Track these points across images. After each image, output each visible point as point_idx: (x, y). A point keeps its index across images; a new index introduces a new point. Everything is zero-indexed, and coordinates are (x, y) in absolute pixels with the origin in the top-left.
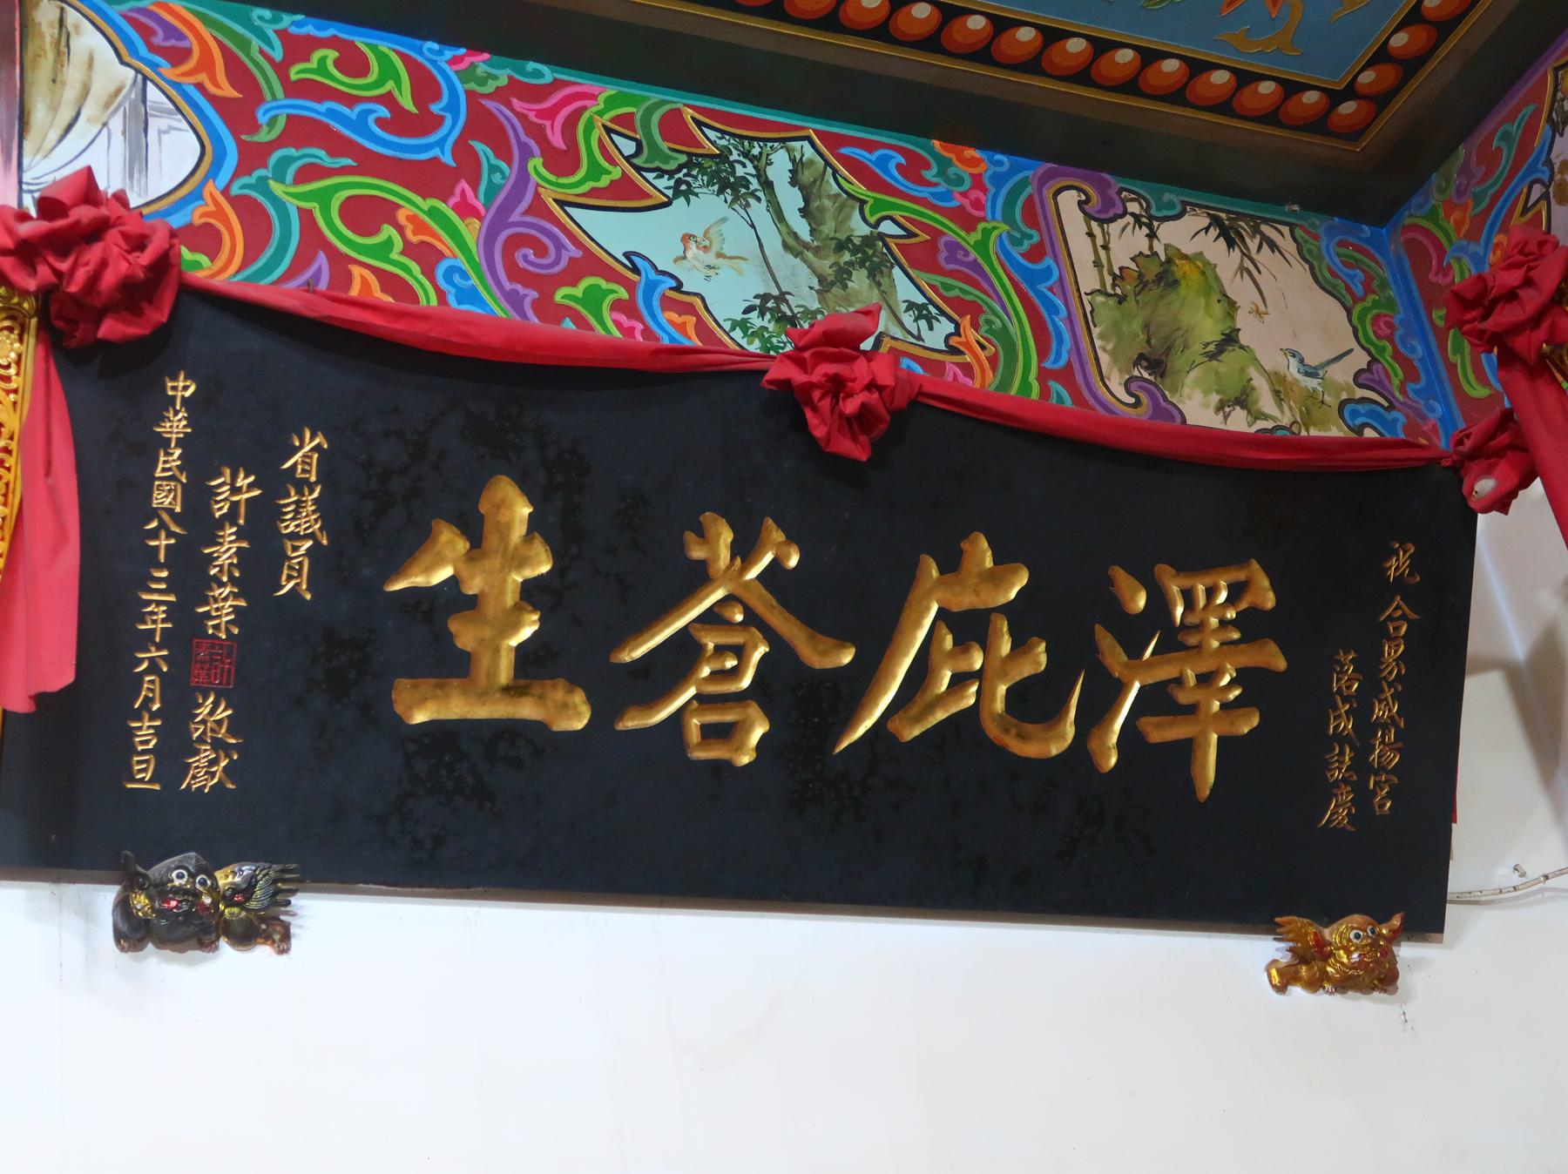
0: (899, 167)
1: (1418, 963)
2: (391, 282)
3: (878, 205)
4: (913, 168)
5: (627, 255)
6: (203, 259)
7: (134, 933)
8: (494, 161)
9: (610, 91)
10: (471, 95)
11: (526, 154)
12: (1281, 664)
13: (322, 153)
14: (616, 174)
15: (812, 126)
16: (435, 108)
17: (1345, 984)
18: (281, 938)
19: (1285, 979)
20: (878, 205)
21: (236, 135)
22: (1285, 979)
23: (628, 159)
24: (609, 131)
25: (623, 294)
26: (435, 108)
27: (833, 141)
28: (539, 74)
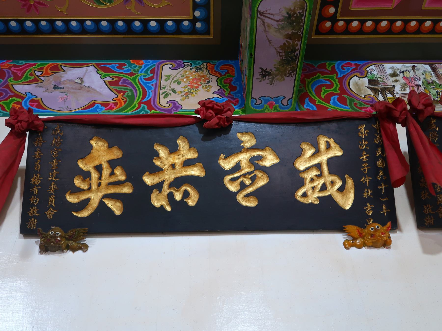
5: (25, 93)
15: (94, 62)
18: (84, 248)
20: (105, 75)
22: (347, 245)
23: (38, 76)
25: (20, 100)
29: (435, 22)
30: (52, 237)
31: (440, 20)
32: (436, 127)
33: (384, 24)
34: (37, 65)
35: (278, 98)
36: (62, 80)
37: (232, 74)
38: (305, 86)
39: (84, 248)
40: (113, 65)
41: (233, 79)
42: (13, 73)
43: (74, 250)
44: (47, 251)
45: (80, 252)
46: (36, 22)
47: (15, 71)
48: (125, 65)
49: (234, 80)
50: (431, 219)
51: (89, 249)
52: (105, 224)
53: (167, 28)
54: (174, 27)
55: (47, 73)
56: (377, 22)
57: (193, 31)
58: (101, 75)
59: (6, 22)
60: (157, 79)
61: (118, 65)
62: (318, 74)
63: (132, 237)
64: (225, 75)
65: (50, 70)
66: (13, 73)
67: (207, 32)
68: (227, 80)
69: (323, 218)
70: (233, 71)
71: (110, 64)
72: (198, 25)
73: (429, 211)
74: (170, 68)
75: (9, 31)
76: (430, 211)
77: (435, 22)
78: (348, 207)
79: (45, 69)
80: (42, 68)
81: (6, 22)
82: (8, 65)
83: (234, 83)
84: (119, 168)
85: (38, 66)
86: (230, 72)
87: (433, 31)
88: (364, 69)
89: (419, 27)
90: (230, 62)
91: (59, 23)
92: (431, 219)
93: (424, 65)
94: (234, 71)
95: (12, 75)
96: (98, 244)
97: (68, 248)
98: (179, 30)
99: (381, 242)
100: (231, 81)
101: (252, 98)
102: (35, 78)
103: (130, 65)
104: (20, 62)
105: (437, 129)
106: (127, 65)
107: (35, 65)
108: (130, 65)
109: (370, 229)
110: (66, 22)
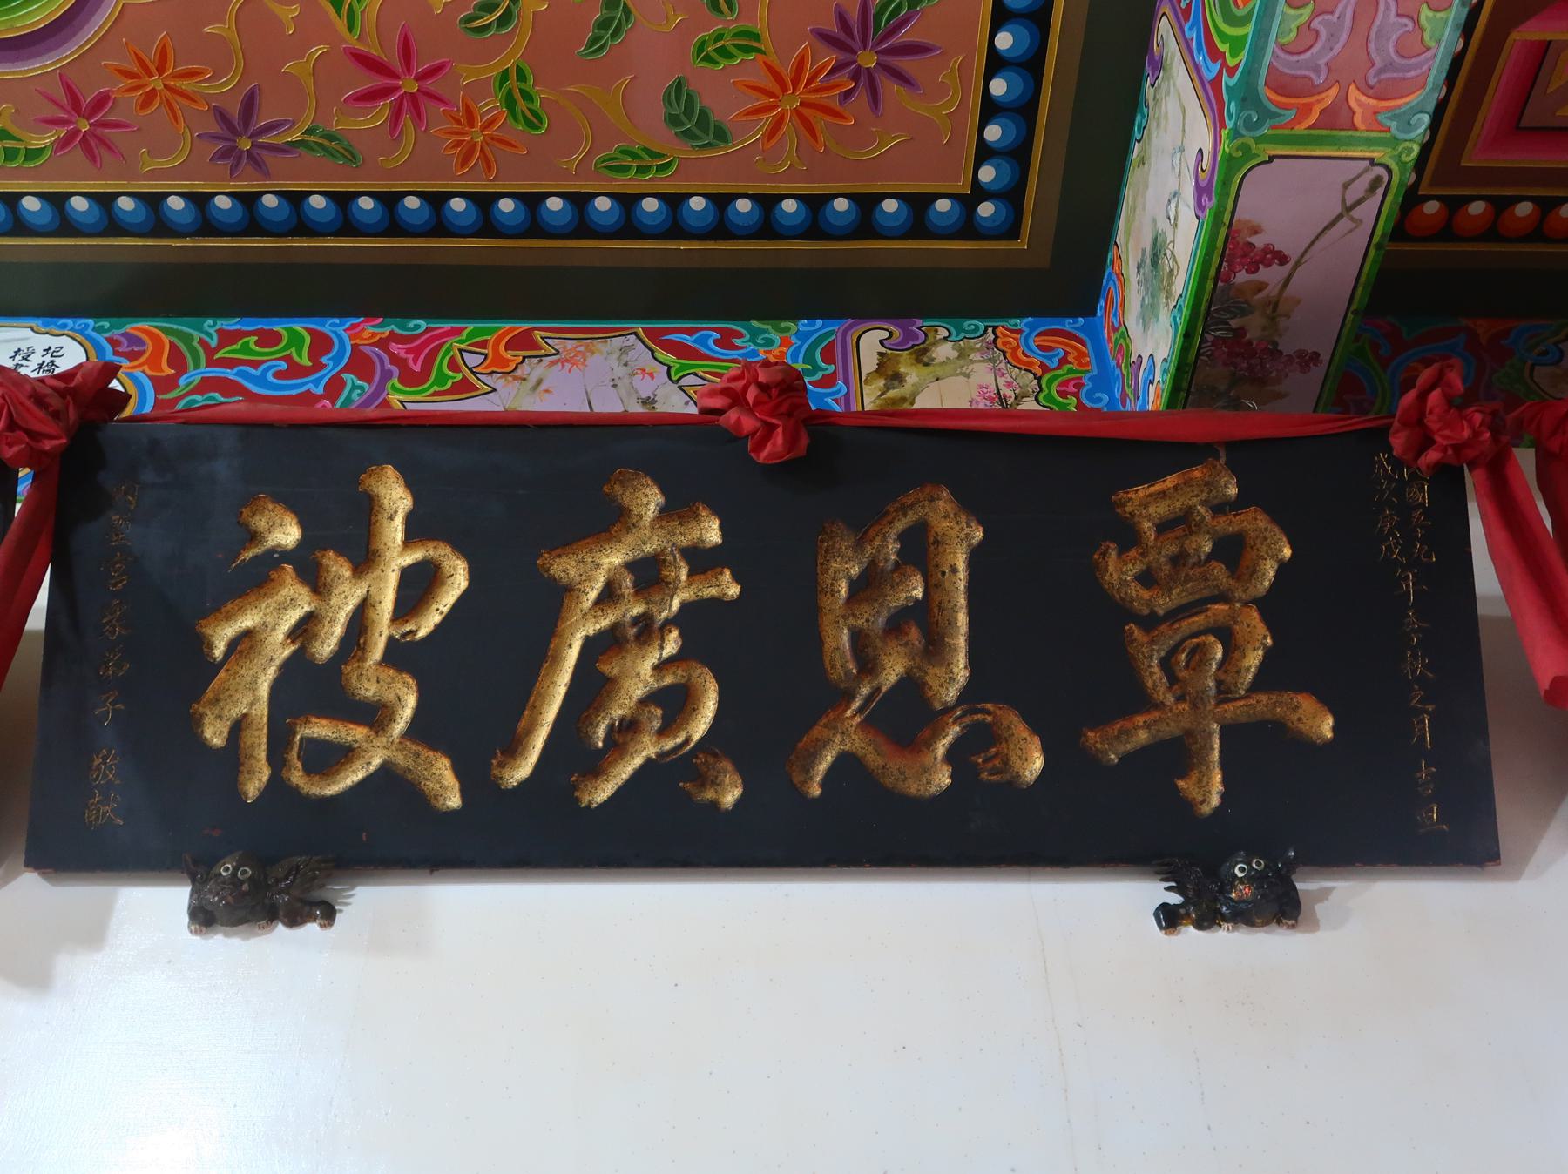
0: (716, 342)
1: (1324, 894)
2: (1155, 685)
3: (683, 367)
4: (726, 340)
6: (399, 536)
7: (203, 917)
8: (237, 347)
9: (471, 326)
10: (355, 347)
11: (387, 376)
12: (734, 590)
13: (217, 395)
14: (459, 376)
15: (639, 326)
16: (324, 360)
17: (1244, 916)
18: (328, 914)
19: (1169, 918)
20: (683, 367)
21: (157, 392)
22: (1169, 918)
24: (461, 351)
26: (324, 360)
27: (653, 335)
28: (418, 327)
29: (1546, 206)
31: (1562, 201)
33: (1524, 209)
34: (465, 333)
37: (1080, 364)
39: (328, 914)
40: (706, 335)
41: (1085, 380)
42: (395, 359)
43: (294, 921)
45: (312, 928)
46: (104, 200)
47: (403, 354)
48: (741, 336)
49: (1088, 386)
52: (401, 837)
53: (360, 217)
54: (756, 216)
55: (500, 361)
56: (1501, 205)
57: (968, 228)
58: (669, 368)
59: (12, 200)
60: (846, 382)
61: (716, 336)
63: (525, 879)
64: (1059, 368)
65: (506, 349)
66: (395, 359)
68: (1065, 383)
70: (1081, 355)
71: (690, 332)
72: (986, 209)
74: (881, 342)
75: (19, 226)
77: (1546, 206)
79: (490, 345)
80: (483, 344)
81: (12, 200)
82: (373, 335)
83: (1089, 396)
85: (470, 336)
86: (1070, 358)
87: (1537, 231)
90: (1068, 324)
91: (126, 204)
94: (1085, 355)
95: (395, 369)
96: (369, 902)
98: (675, 227)
100: (1079, 386)
102: (464, 379)
103: (755, 333)
104: (412, 323)
106: (748, 337)
107: (458, 331)
108: (755, 333)
110: (580, 201)
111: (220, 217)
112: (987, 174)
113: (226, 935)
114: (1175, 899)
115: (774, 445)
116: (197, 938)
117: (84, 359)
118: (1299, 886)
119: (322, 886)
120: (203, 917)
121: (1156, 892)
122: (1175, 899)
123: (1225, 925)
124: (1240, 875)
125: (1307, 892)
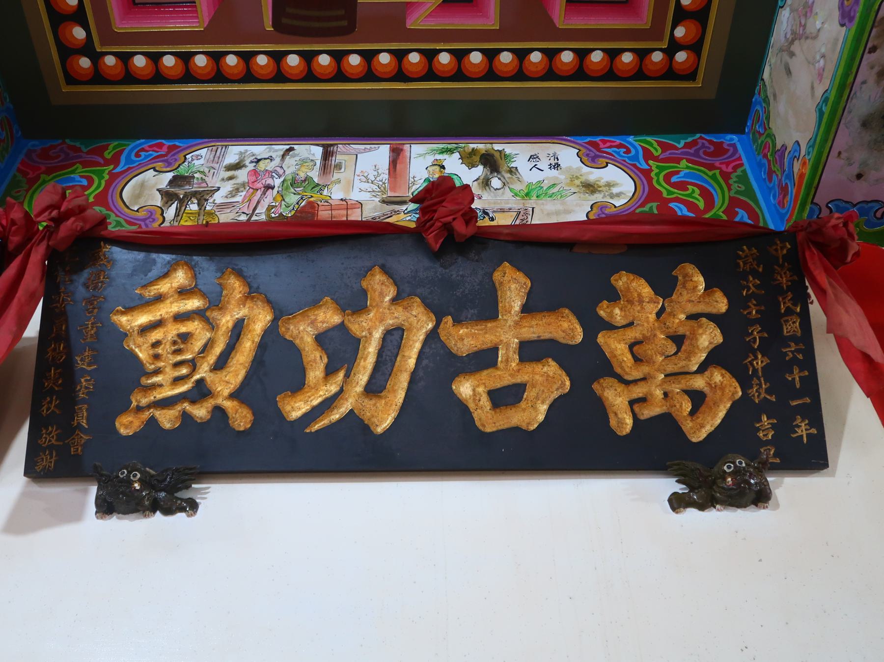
18: (192, 506)
22: (677, 503)
30: (122, 481)
32: (759, 267)
35: (870, 205)
36: (481, 167)
38: (27, 191)
39: (192, 506)
43: (168, 511)
44: (111, 513)
45: (181, 516)
50: (51, 458)
51: (200, 507)
62: (78, 165)
63: (219, 483)
67: (71, 80)
69: (650, 448)
73: (50, 441)
76: (53, 441)
78: (380, 430)
84: (719, 339)
88: (182, 155)
89: (521, 66)
92: (51, 458)
93: (312, 147)
96: (218, 497)
97: (155, 507)
99: (753, 496)
101: (812, 202)
105: (761, 270)
109: (725, 468)
111: (228, 70)
112: (110, 60)
113: (118, 518)
114: (679, 488)
115: (592, 173)
116: (100, 521)
117: (321, 149)
118: (769, 479)
119: (188, 487)
120: (106, 507)
121: (669, 485)
122: (679, 488)
123: (718, 506)
124: (728, 471)
125: (86, 492)
